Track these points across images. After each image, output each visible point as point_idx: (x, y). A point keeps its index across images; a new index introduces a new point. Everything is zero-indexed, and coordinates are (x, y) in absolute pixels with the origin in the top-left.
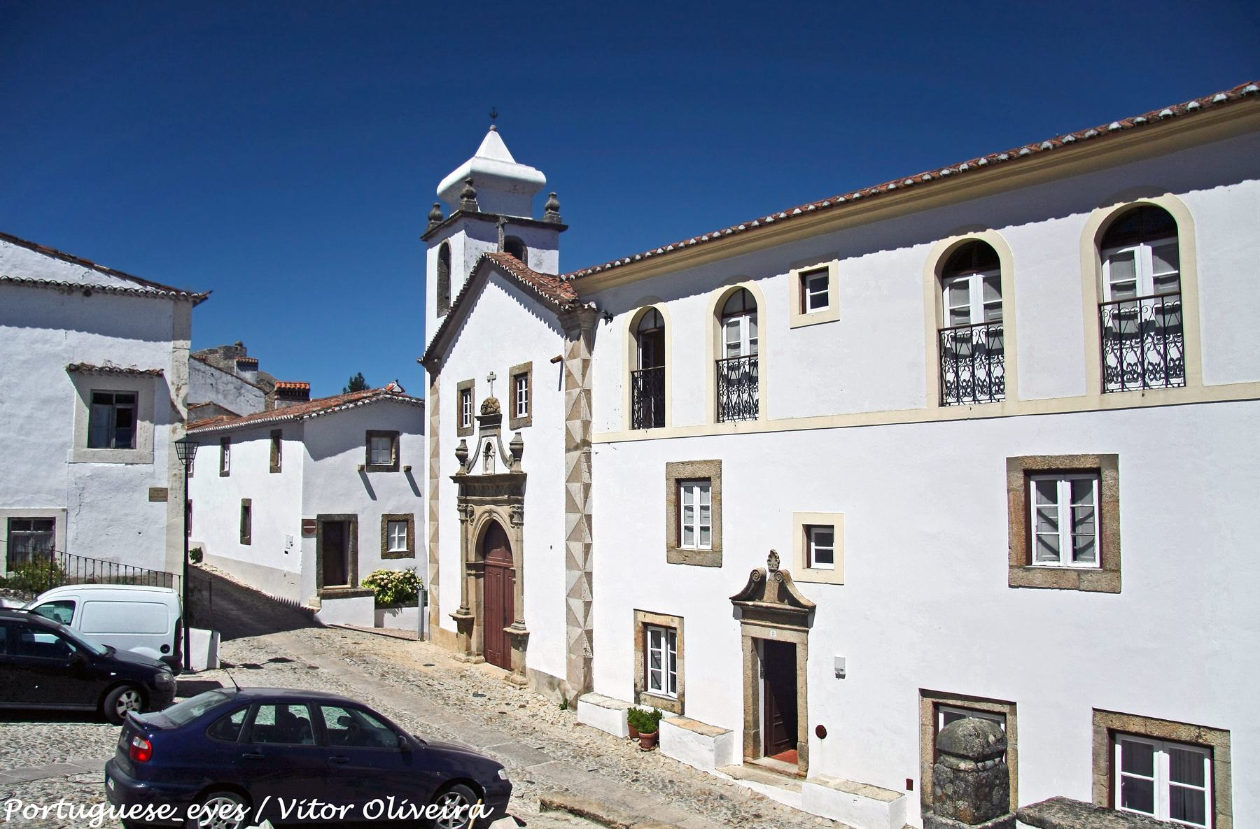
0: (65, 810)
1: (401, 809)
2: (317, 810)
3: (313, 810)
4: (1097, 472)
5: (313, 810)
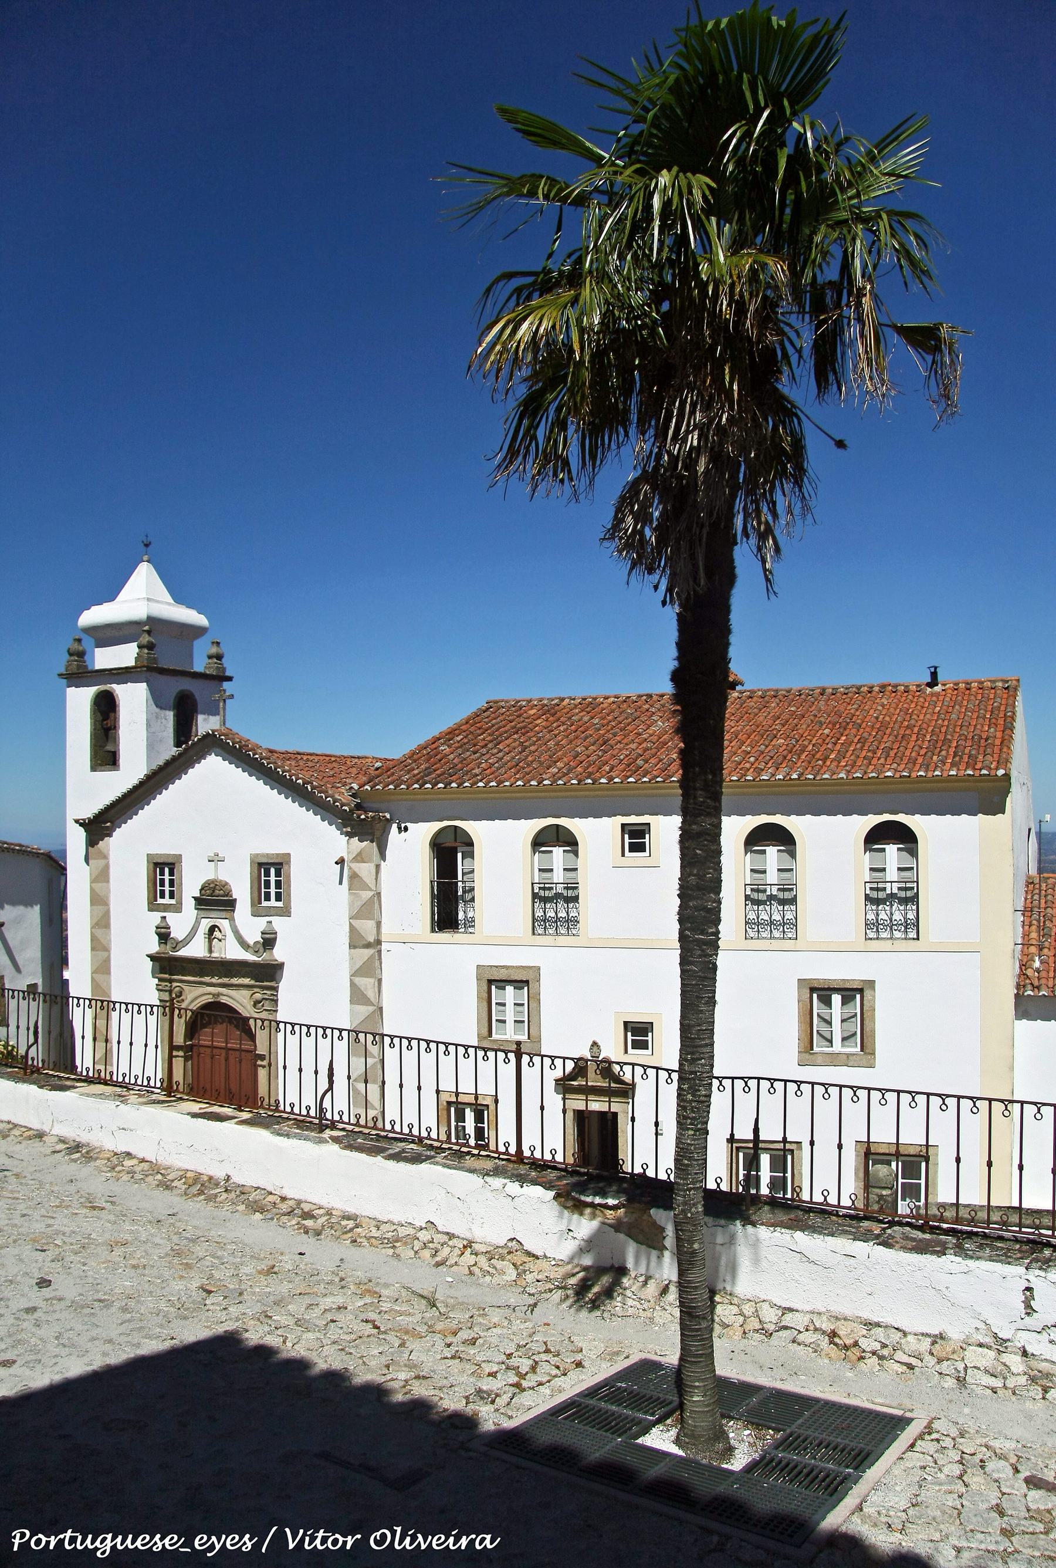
0: (73, 1540)
1: (408, 1539)
2: (324, 1540)
3: (320, 1541)
4: (861, 991)
5: (320, 1541)
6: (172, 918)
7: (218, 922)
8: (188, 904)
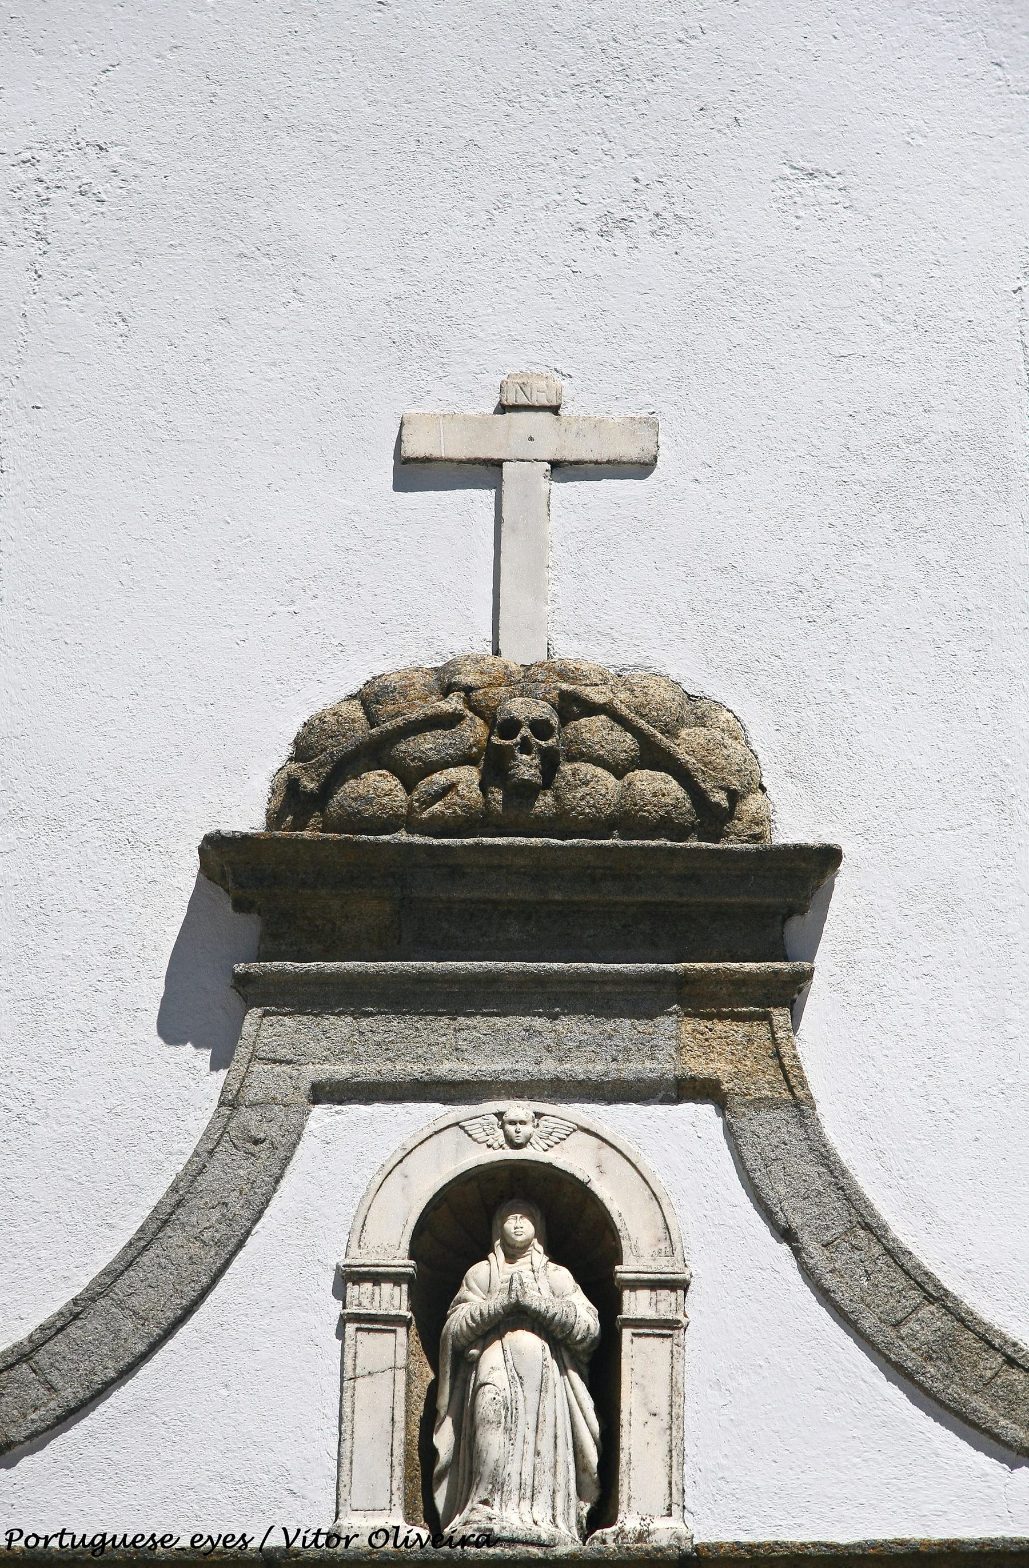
7: (567, 1141)
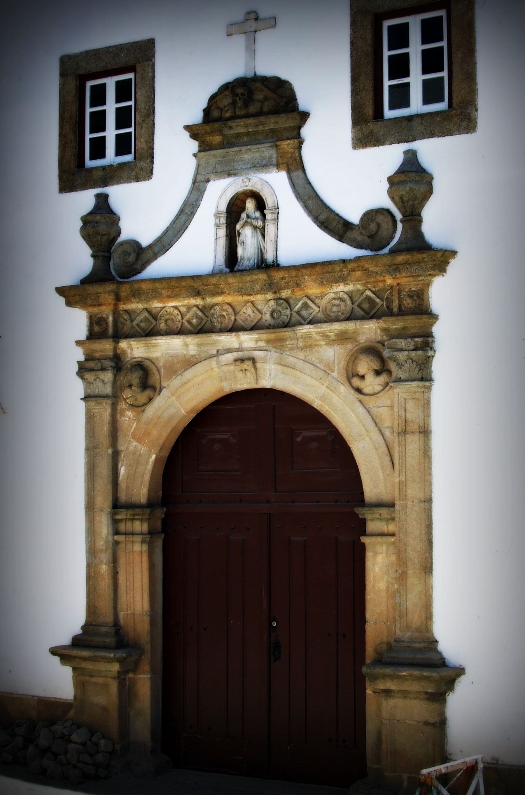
6: (120, 195)
8: (174, 152)
